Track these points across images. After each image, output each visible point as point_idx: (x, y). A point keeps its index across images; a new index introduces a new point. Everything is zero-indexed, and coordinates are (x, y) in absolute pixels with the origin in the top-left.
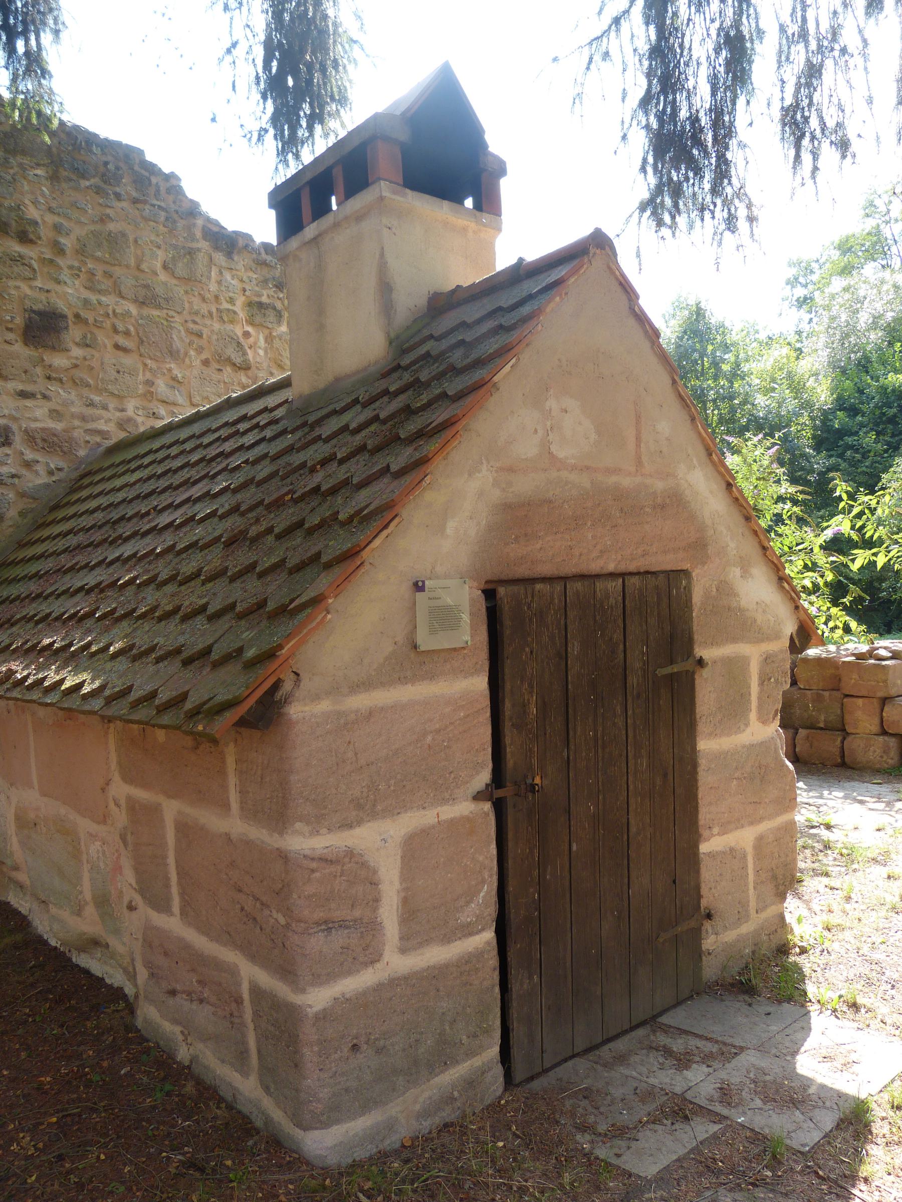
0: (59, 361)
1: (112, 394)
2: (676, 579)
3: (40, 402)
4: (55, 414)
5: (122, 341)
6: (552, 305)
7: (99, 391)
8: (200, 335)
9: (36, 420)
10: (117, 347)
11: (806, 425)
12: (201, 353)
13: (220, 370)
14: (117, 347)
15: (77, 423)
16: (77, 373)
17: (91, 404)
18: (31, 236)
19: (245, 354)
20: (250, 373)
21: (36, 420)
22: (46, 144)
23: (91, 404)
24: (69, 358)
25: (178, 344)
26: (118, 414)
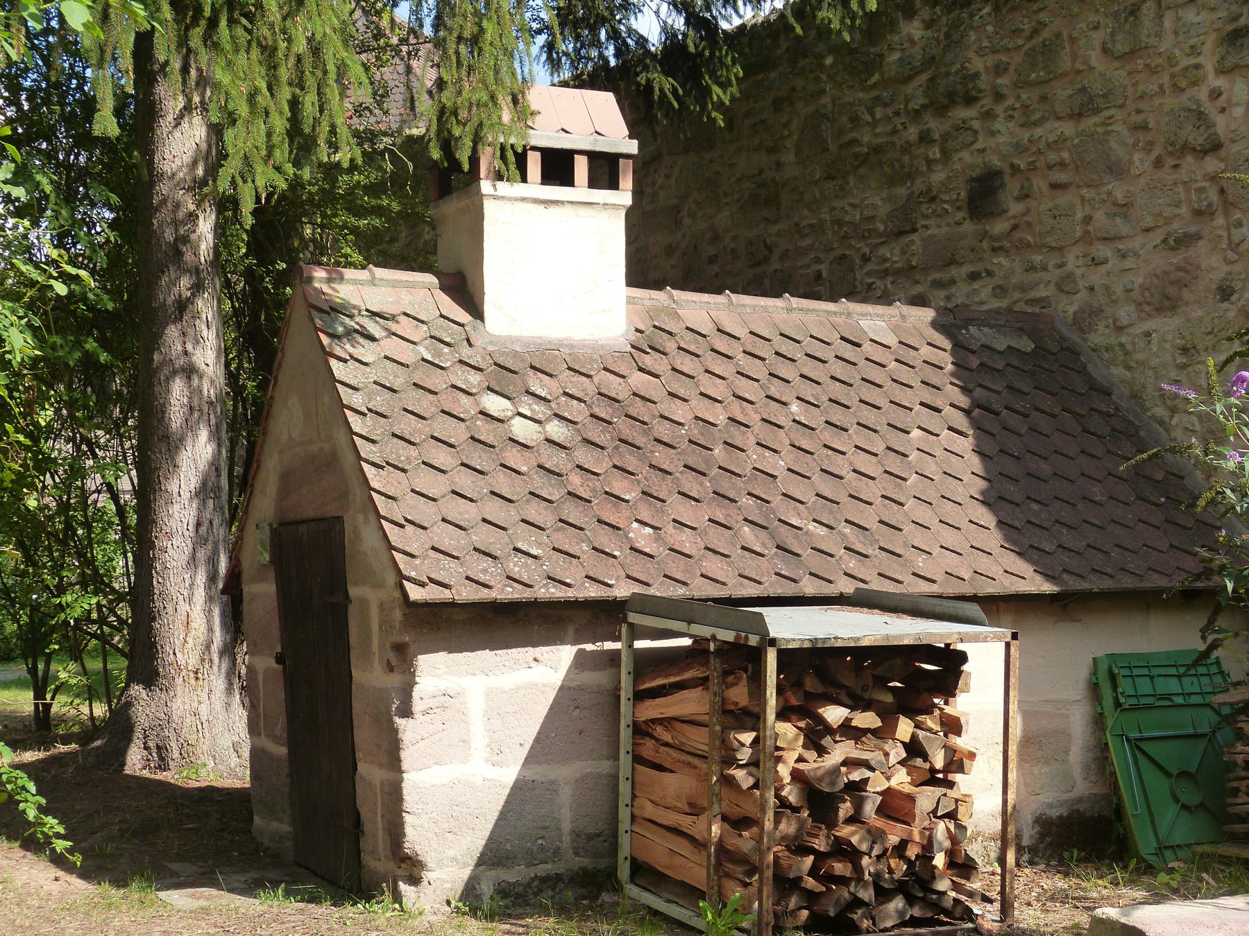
0: (999, 227)
1: (1052, 249)
2: (339, 519)
3: (987, 280)
4: (1000, 291)
5: (1061, 177)
6: (363, 275)
7: (1037, 248)
8: (1144, 127)
9: (982, 303)
10: (1055, 186)
11: (1014, 109)
12: (1150, 151)
13: (1176, 166)
14: (1055, 186)
15: (1017, 295)
16: (1018, 235)
17: (1031, 268)
18: (974, 93)
19: (1210, 125)
20: (1223, 152)
21: (982, 303)
22: (845, 41)
23: (1031, 268)
24: (1008, 219)
25: (1119, 151)
26: (1058, 272)
